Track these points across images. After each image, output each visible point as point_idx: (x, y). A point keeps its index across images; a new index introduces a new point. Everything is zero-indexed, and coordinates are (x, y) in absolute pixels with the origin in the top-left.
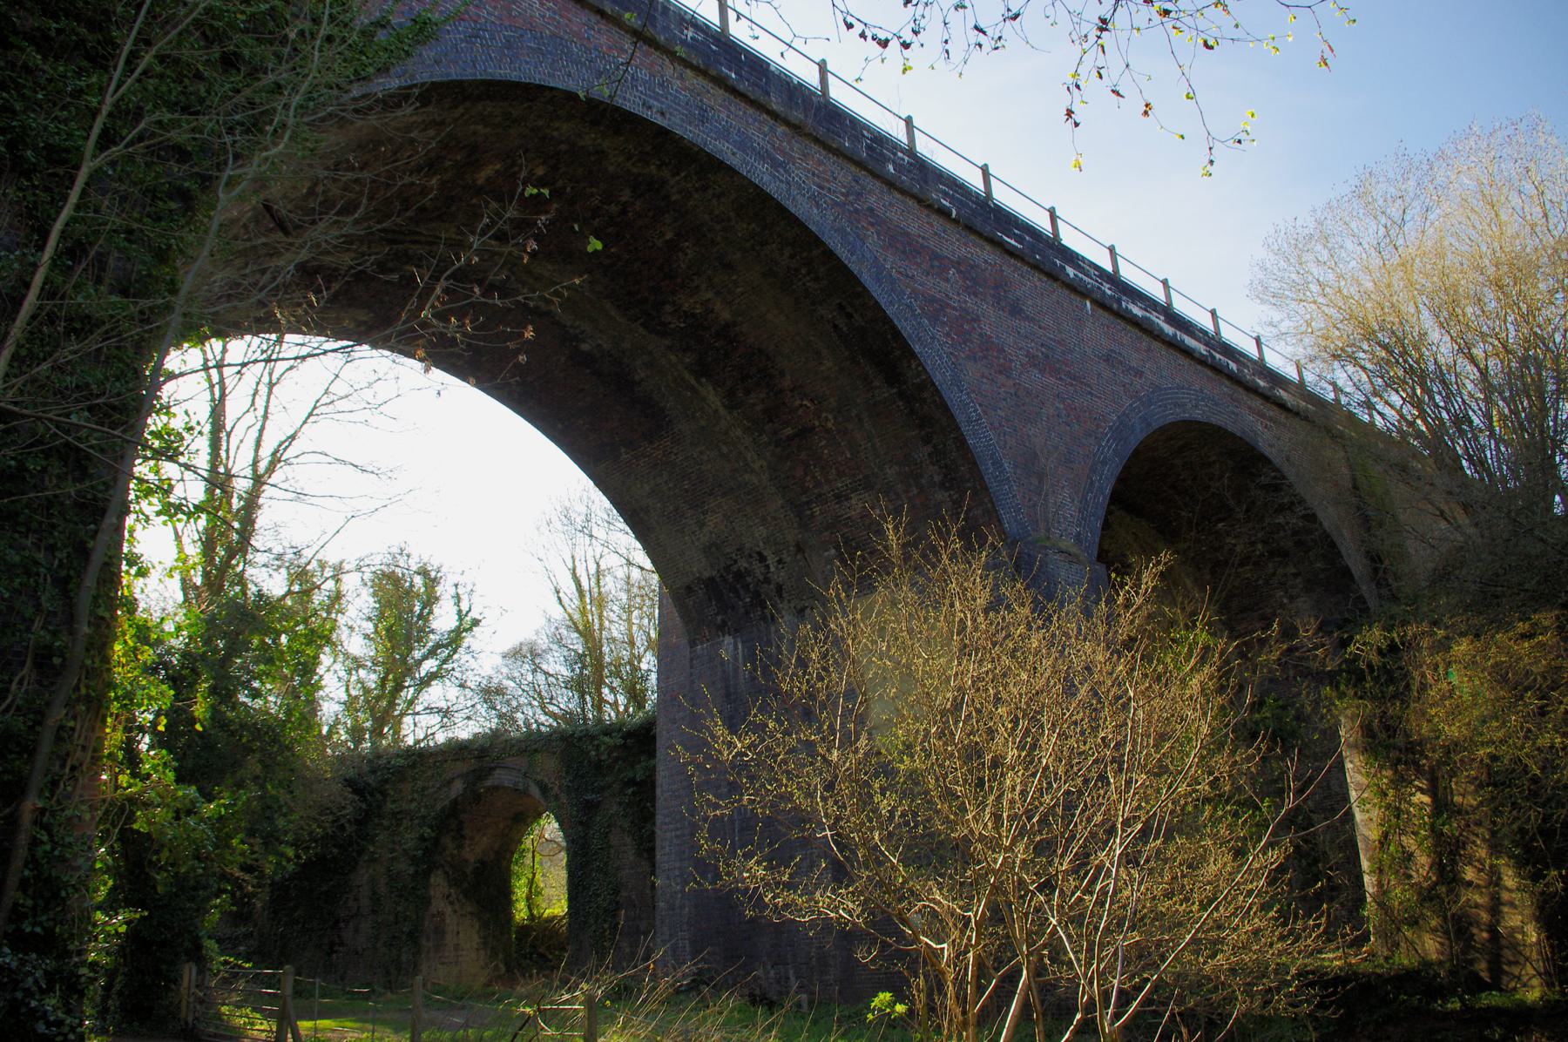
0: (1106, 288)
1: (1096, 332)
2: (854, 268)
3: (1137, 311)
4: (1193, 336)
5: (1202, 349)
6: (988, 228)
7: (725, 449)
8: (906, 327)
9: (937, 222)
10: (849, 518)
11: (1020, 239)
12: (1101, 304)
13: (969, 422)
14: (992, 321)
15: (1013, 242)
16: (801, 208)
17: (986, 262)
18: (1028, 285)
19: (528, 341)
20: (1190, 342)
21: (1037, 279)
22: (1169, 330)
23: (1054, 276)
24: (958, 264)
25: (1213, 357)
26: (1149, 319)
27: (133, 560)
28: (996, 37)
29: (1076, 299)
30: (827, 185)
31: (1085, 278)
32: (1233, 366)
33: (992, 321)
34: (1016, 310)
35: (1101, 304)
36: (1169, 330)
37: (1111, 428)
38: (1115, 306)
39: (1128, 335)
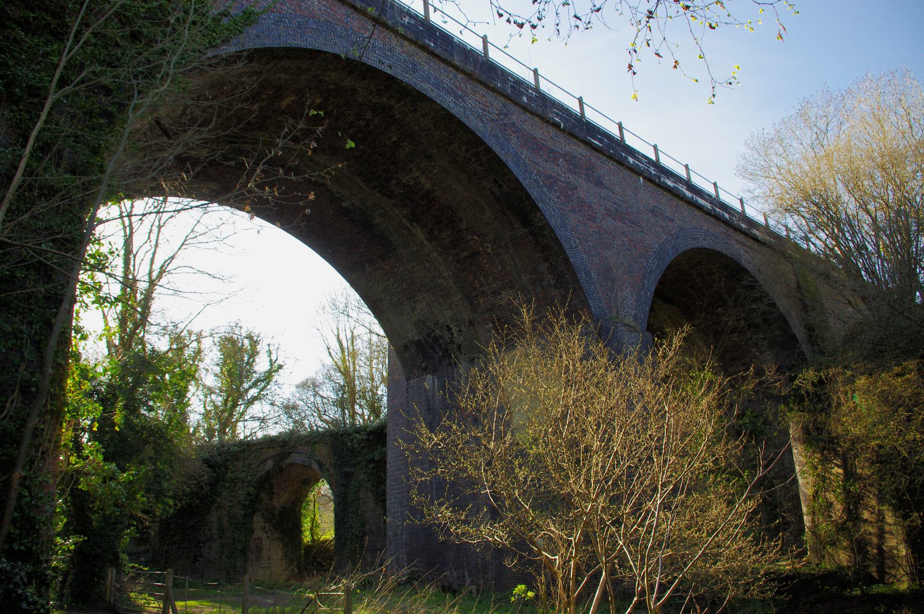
0: (652, 170)
1: (646, 196)
2: (503, 158)
3: (670, 183)
4: (703, 198)
5: (708, 206)
6: (582, 135)
7: (427, 265)
8: (534, 193)
9: (552, 131)
10: (500, 305)
11: (601, 141)
12: (649, 179)
13: (571, 248)
14: (585, 189)
15: (597, 143)
16: (472, 122)
17: (581, 154)
18: (606, 168)
19: (311, 201)
20: (701, 201)
21: (611, 165)
22: (689, 194)
23: (621, 163)
24: (564, 155)
25: (715, 211)
26: (677, 188)
27: (78, 330)
28: (587, 22)
29: (634, 176)
30: (487, 109)
31: (639, 164)
32: (726, 215)
33: (585, 189)
34: (598, 183)
35: (649, 179)
36: (689, 194)
37: (655, 252)
38: (657, 180)
39: (665, 198)
